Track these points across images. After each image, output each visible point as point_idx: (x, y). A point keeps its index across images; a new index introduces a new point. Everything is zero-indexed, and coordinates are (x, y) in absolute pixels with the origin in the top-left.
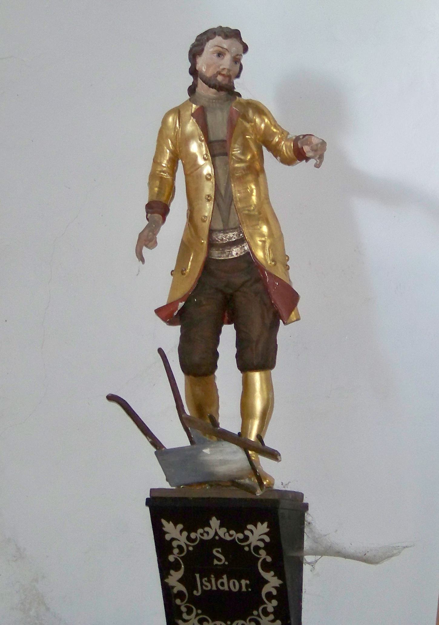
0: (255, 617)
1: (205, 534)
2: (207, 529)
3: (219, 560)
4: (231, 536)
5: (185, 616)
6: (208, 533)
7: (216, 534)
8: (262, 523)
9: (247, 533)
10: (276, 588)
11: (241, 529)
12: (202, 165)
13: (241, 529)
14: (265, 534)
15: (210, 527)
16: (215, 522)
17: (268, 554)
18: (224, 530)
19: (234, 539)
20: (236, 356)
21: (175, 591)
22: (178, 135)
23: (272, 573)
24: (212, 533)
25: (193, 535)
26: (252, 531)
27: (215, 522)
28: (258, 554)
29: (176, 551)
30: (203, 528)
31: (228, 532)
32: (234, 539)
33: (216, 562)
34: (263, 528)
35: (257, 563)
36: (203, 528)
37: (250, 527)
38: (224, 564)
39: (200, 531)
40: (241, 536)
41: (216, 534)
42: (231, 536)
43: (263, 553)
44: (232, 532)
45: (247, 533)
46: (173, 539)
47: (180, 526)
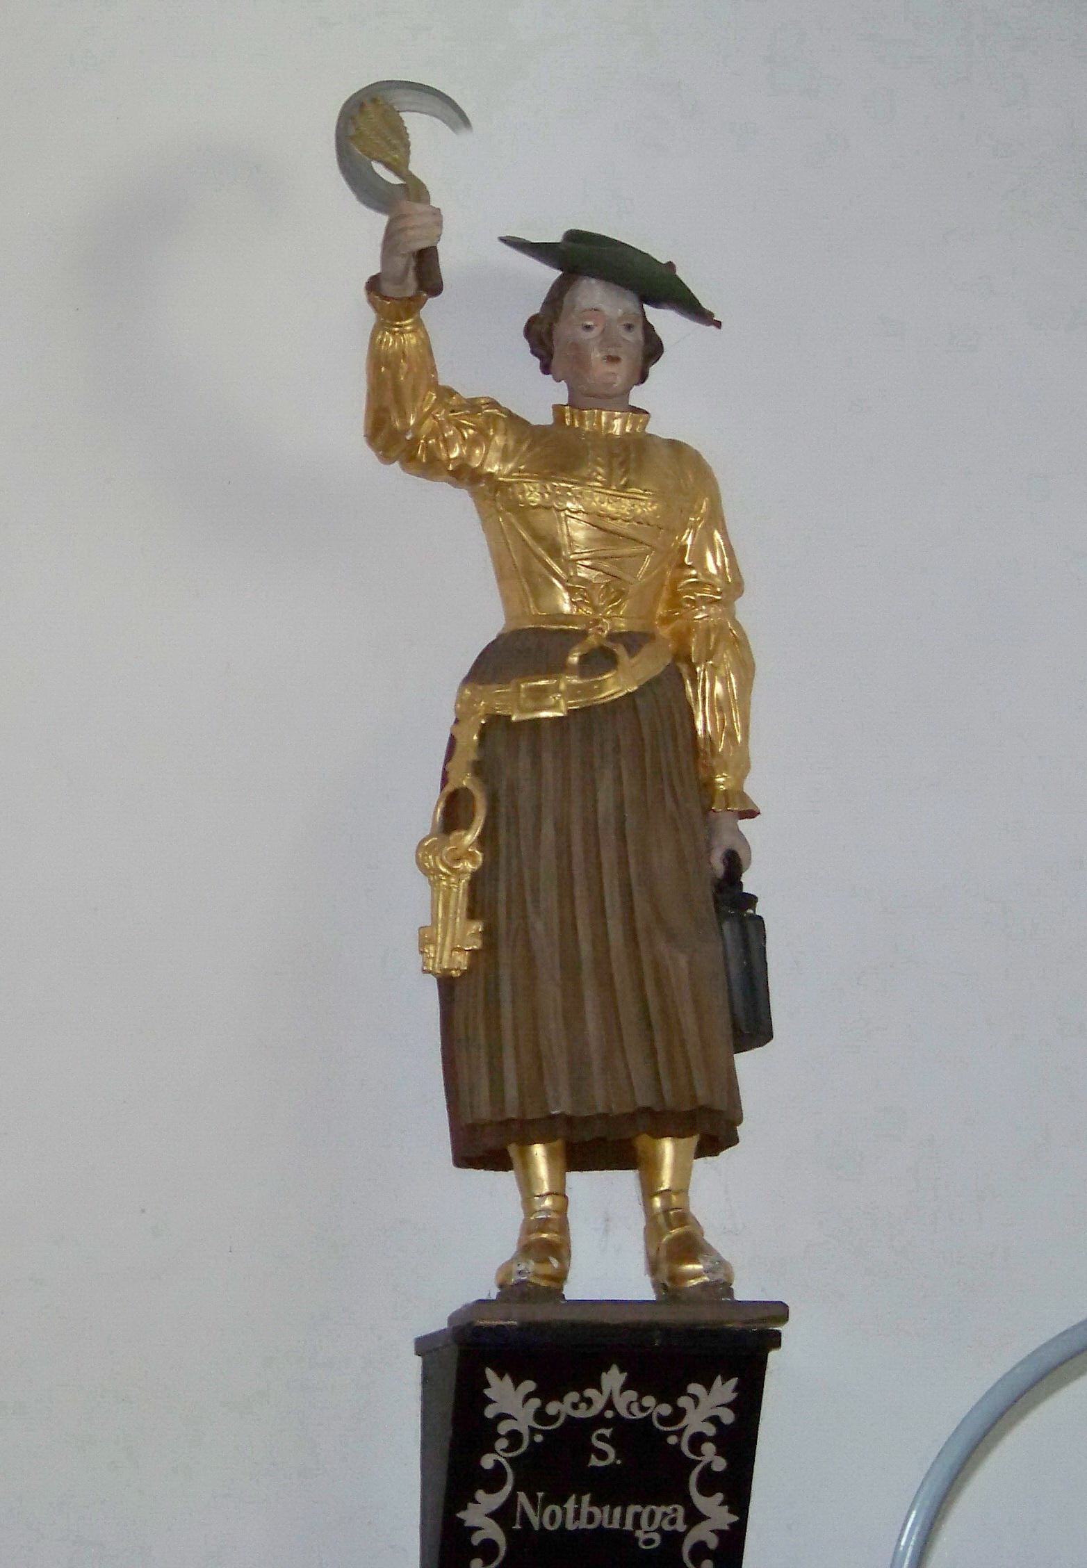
0: (669, 1429)
1: (583, 1405)
2: (590, 1393)
3: (602, 1455)
4: (643, 1409)
5: (535, 1403)
6: (589, 1402)
7: (610, 1405)
8: (725, 1380)
9: (683, 1402)
10: (719, 1533)
11: (670, 1391)
12: (435, 975)
13: (670, 1391)
14: (728, 1405)
15: (598, 1387)
16: (613, 1379)
17: (719, 1453)
18: (632, 1395)
19: (648, 1419)
20: (752, 895)
21: (476, 1539)
22: (683, 1043)
23: (719, 1497)
24: (599, 1402)
25: (552, 1408)
26: (696, 1399)
27: (613, 1379)
28: (699, 1454)
29: (502, 1444)
30: (580, 1391)
31: (639, 1400)
32: (648, 1419)
33: (594, 1461)
34: (724, 1390)
35: (688, 1476)
36: (580, 1390)
37: (695, 1388)
38: (614, 1464)
39: (573, 1397)
40: (666, 1409)
41: (610, 1405)
42: (643, 1409)
43: (708, 1449)
44: (649, 1401)
45: (683, 1402)
46: (502, 1417)
47: (529, 1386)
